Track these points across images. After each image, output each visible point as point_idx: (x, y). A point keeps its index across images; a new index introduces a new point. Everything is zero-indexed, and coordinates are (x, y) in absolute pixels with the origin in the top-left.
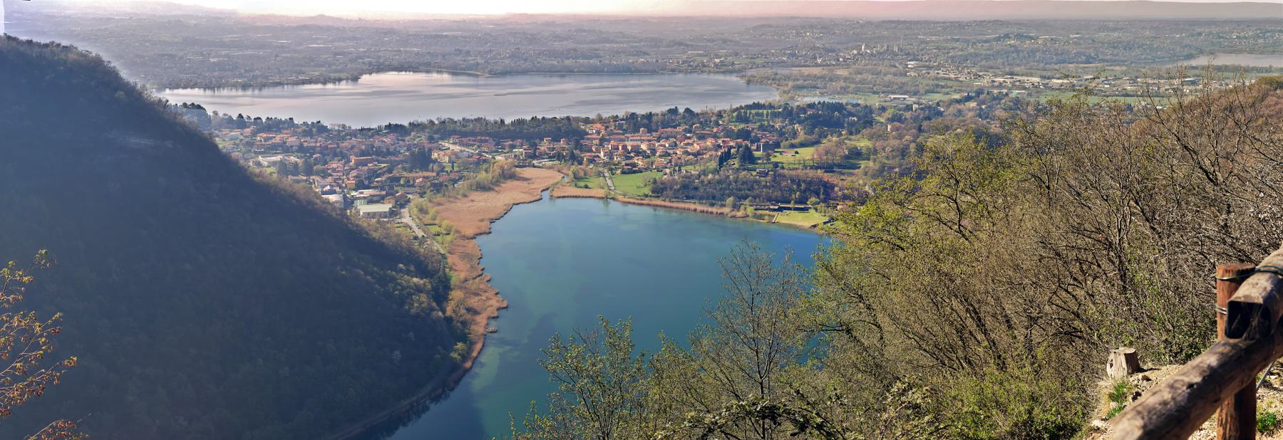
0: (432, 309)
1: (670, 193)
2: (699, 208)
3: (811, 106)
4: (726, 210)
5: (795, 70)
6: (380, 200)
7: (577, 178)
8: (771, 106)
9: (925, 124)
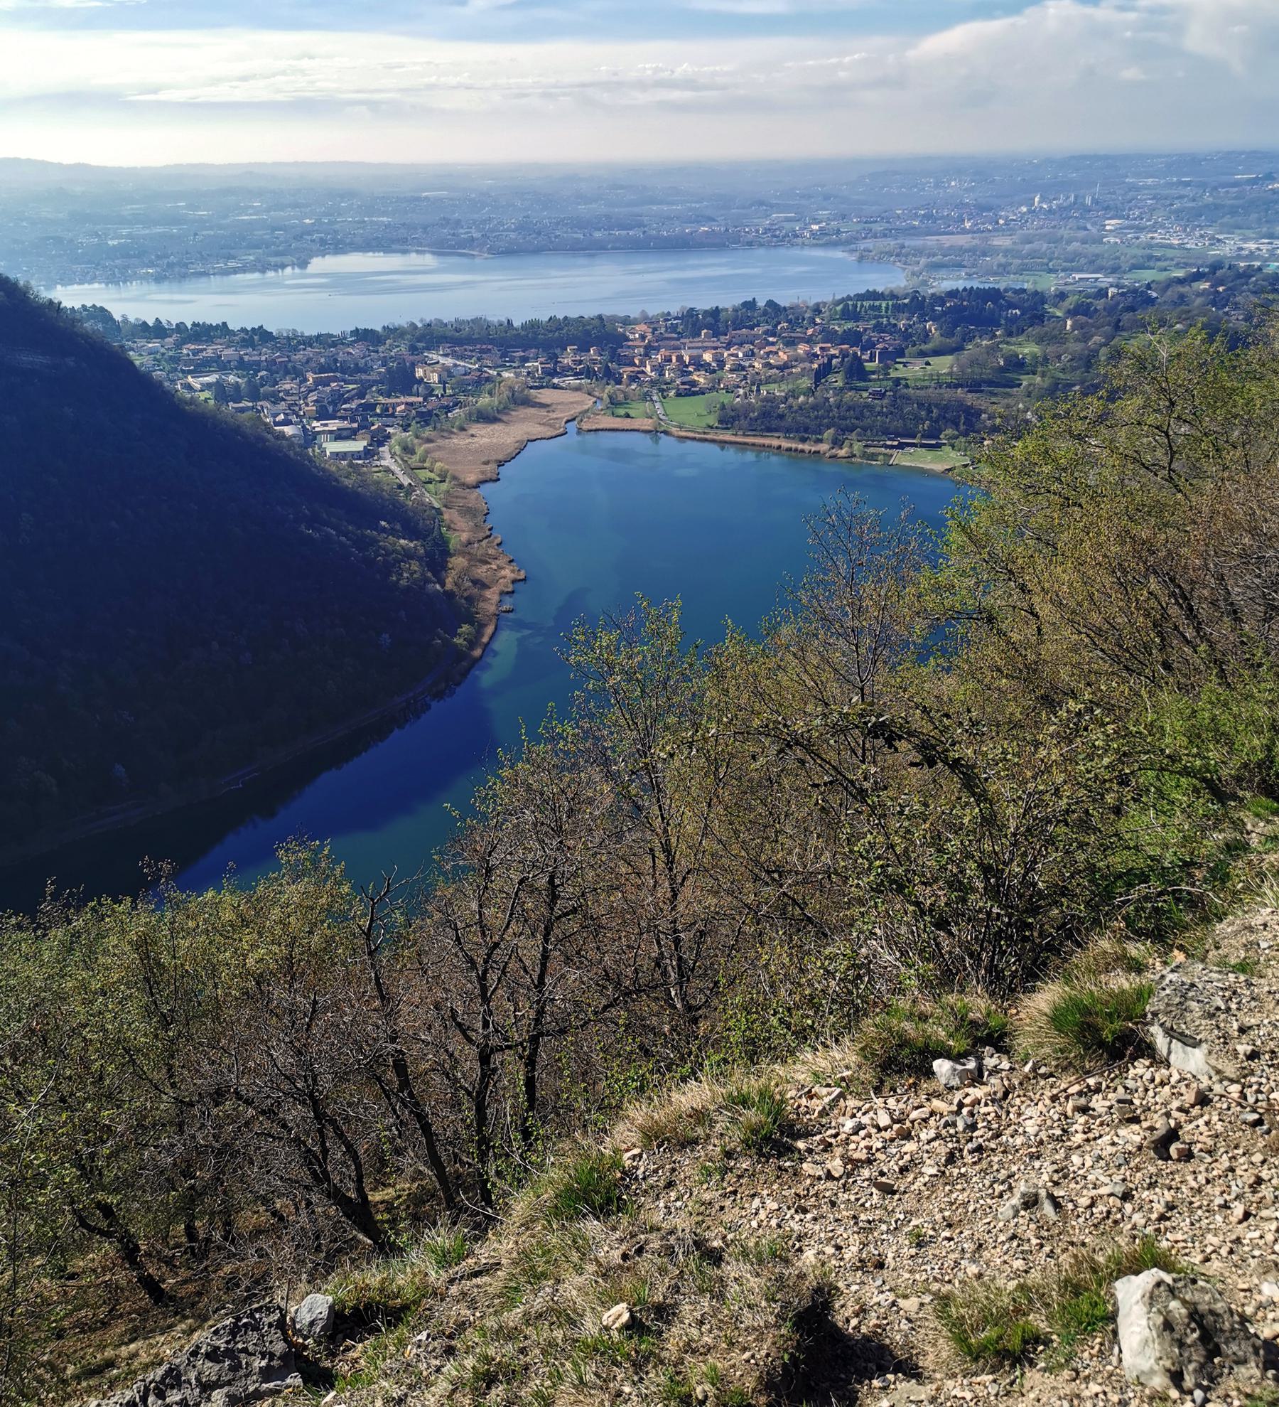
0: (427, 581)
1: (744, 423)
2: (785, 444)
3: (953, 294)
4: (823, 447)
5: (931, 241)
7: (614, 403)
8: (893, 296)
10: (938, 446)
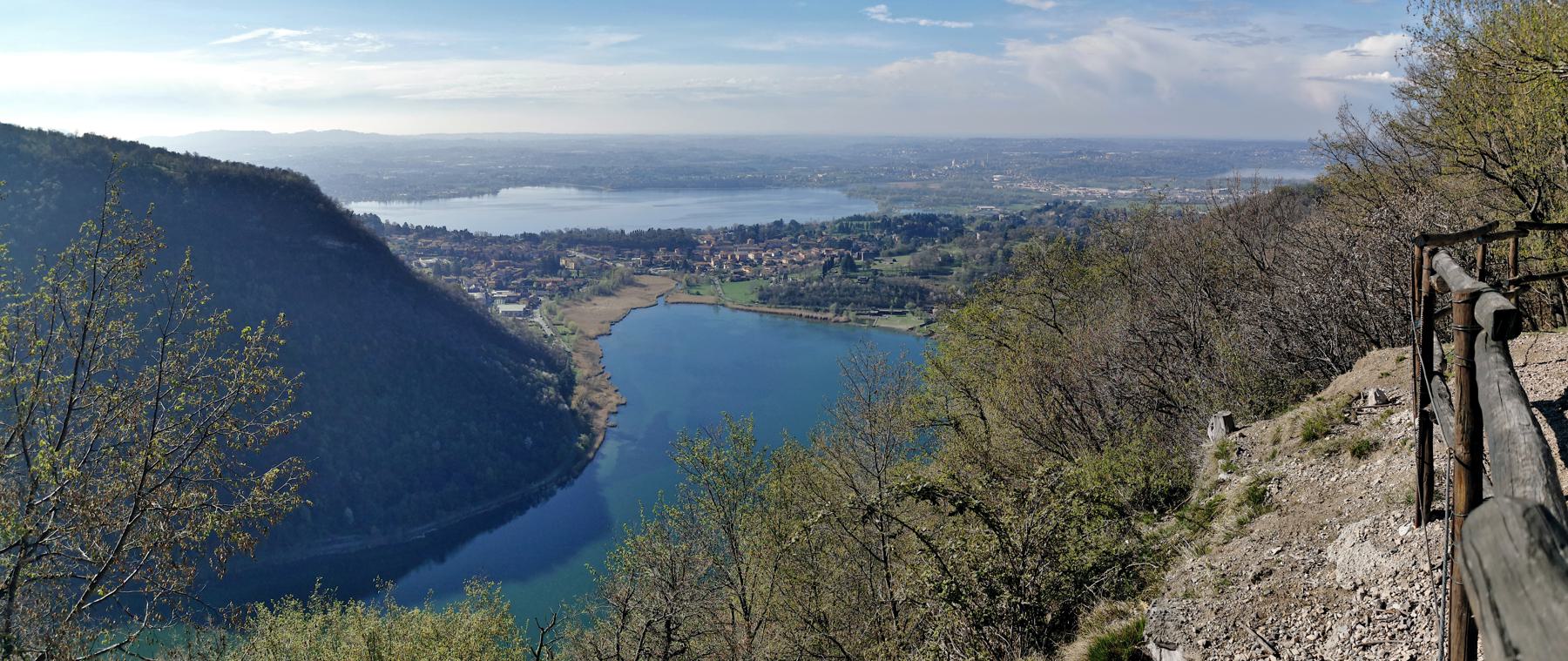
0: (559, 401)
1: (776, 299)
2: (805, 313)
3: (907, 217)
4: (830, 315)
5: (892, 185)
6: (515, 300)
7: (689, 285)
8: (871, 218)
9: (1011, 232)
10: (903, 313)
